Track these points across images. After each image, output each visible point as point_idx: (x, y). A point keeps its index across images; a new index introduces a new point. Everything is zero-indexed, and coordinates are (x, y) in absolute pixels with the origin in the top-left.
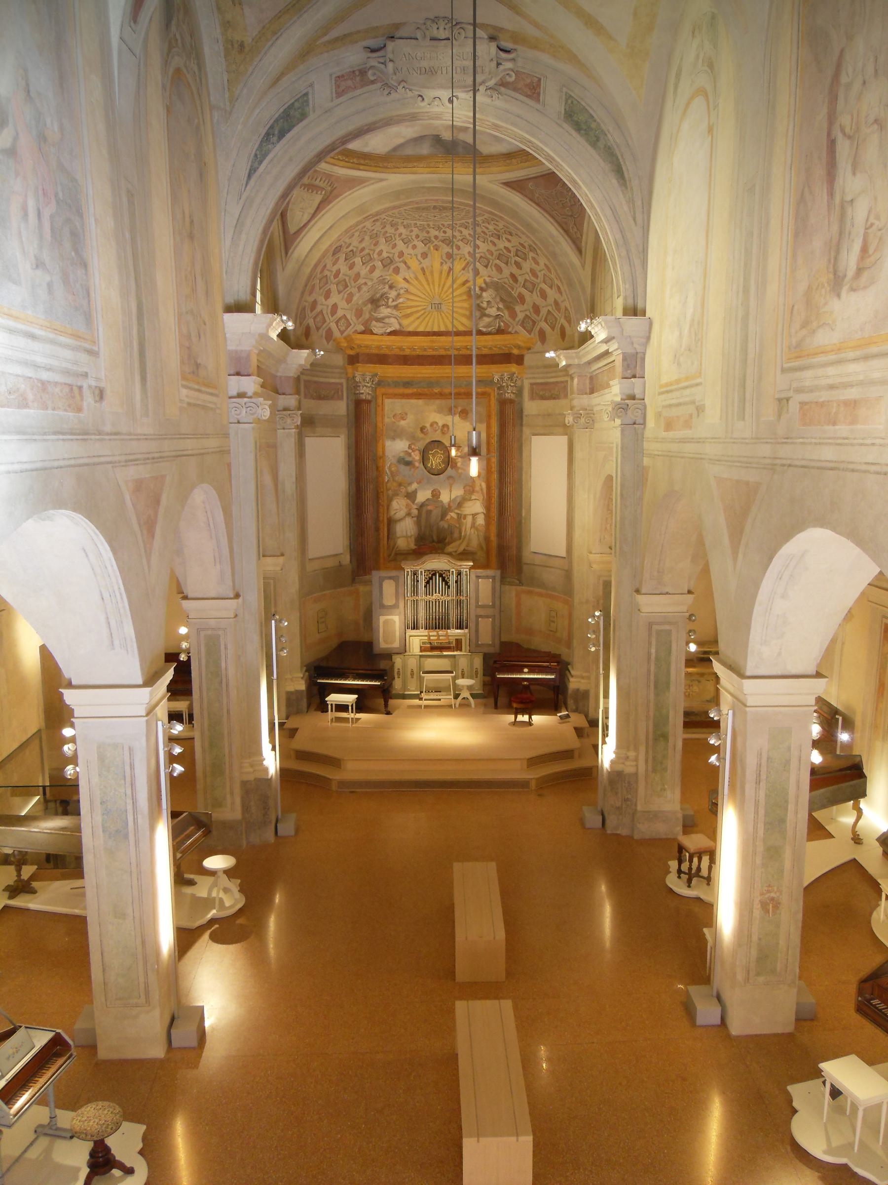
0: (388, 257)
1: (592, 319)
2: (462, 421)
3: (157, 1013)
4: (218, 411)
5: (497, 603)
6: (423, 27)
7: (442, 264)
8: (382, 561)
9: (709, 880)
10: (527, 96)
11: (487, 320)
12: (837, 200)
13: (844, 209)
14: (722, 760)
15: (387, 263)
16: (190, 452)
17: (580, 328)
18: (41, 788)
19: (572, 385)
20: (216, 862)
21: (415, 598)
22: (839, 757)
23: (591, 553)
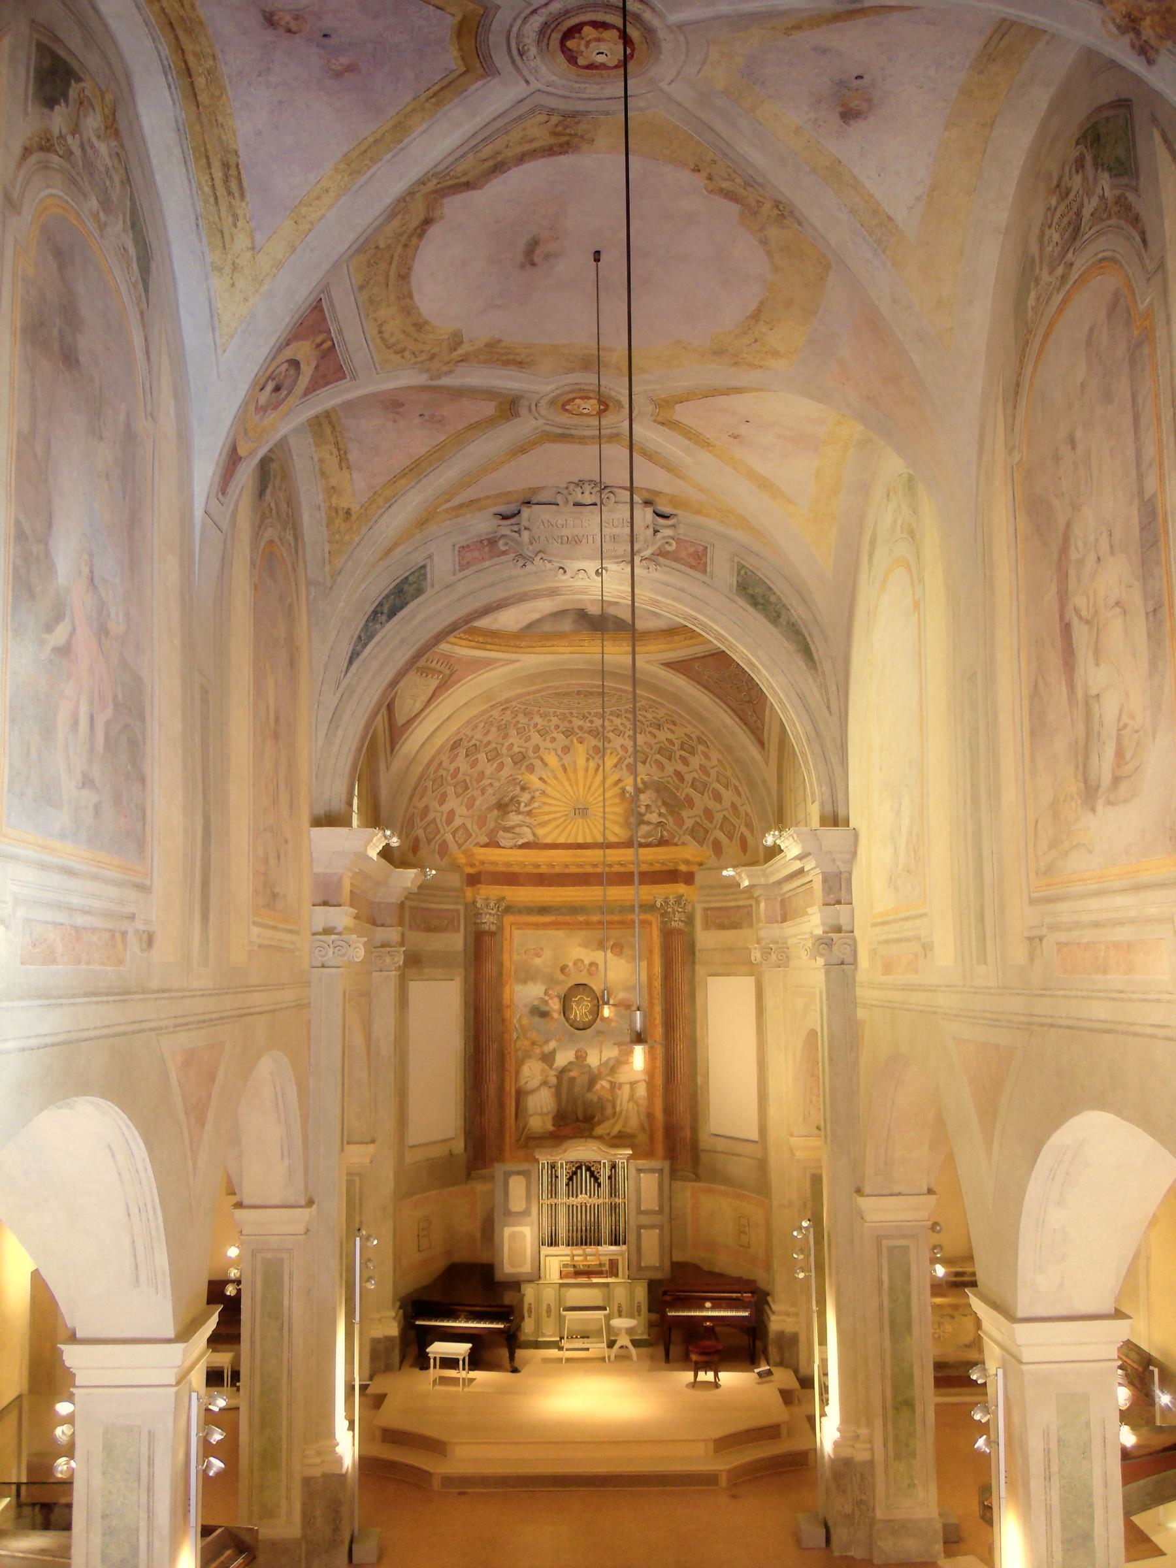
1: (780, 831)
5: (667, 1209)
6: (565, 492)
7: (588, 760)
8: (507, 1148)
10: (692, 567)
11: (645, 829)
13: (1090, 702)
15: (520, 759)
16: (258, 1009)
18: (14, 1487)
21: (553, 1201)
22: (1161, 1430)
23: (792, 1135)
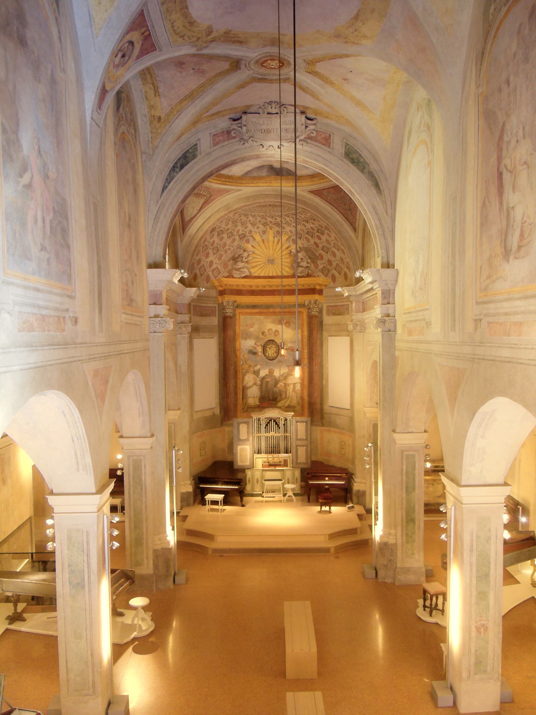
0: (243, 234)
2: (287, 328)
3: (100, 700)
4: (143, 326)
6: (263, 107)
7: (274, 237)
9: (443, 611)
10: (323, 144)
11: (300, 269)
12: (505, 207)
14: (448, 537)
15: (242, 237)
17: (356, 275)
18: (30, 555)
19: (352, 307)
20: (138, 602)
21: (259, 435)
22: (521, 532)
23: (365, 407)
